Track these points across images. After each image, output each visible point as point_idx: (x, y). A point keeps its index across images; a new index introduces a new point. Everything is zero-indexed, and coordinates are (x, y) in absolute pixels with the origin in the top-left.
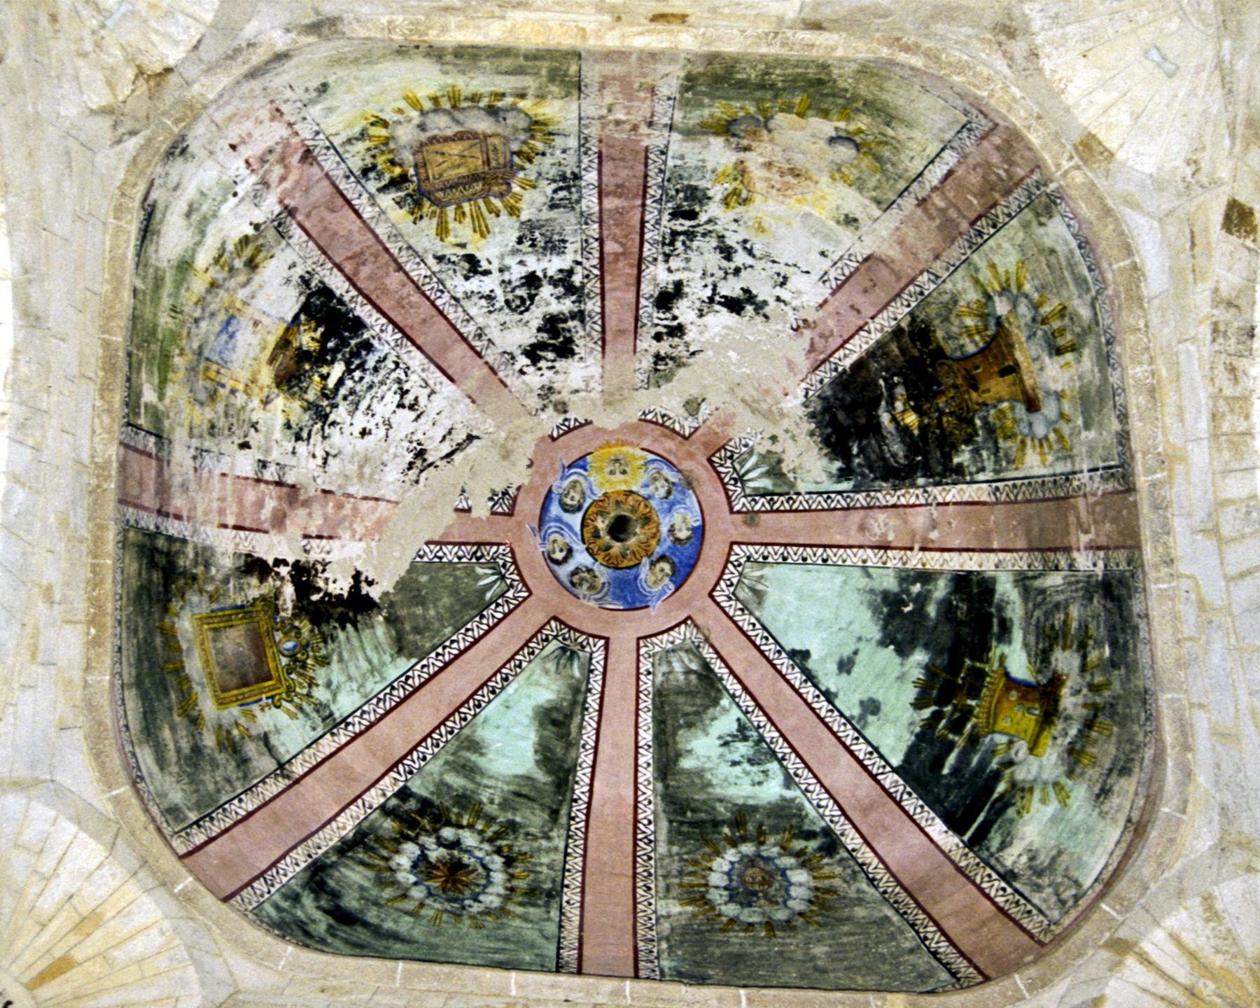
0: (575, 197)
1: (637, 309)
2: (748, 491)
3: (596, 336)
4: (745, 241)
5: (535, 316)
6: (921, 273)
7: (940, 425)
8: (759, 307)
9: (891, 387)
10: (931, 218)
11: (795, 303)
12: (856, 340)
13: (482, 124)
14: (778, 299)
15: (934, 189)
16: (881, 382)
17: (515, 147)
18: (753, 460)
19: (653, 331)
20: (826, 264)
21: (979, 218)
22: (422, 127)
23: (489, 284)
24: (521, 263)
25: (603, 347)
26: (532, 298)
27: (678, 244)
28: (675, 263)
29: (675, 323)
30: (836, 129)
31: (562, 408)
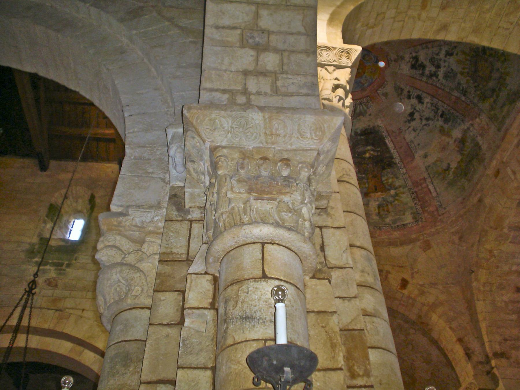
0: (459, 91)
1: (419, 90)
2: (357, 106)
3: (415, 76)
4: (429, 125)
5: (427, 63)
6: (406, 170)
7: (364, 163)
8: (409, 121)
9: (377, 151)
10: (420, 180)
11: (407, 131)
12: (392, 145)
13: (491, 84)
14: (410, 127)
15: (428, 186)
16: (379, 149)
17: (481, 86)
18: (365, 108)
19: (411, 91)
20: (416, 144)
21: (417, 195)
22: (498, 70)
23: (442, 55)
24: (445, 66)
25: (411, 77)
26: (433, 65)
27: (434, 108)
28: (429, 105)
29: (412, 98)
30: (452, 168)
31: (396, 61)
